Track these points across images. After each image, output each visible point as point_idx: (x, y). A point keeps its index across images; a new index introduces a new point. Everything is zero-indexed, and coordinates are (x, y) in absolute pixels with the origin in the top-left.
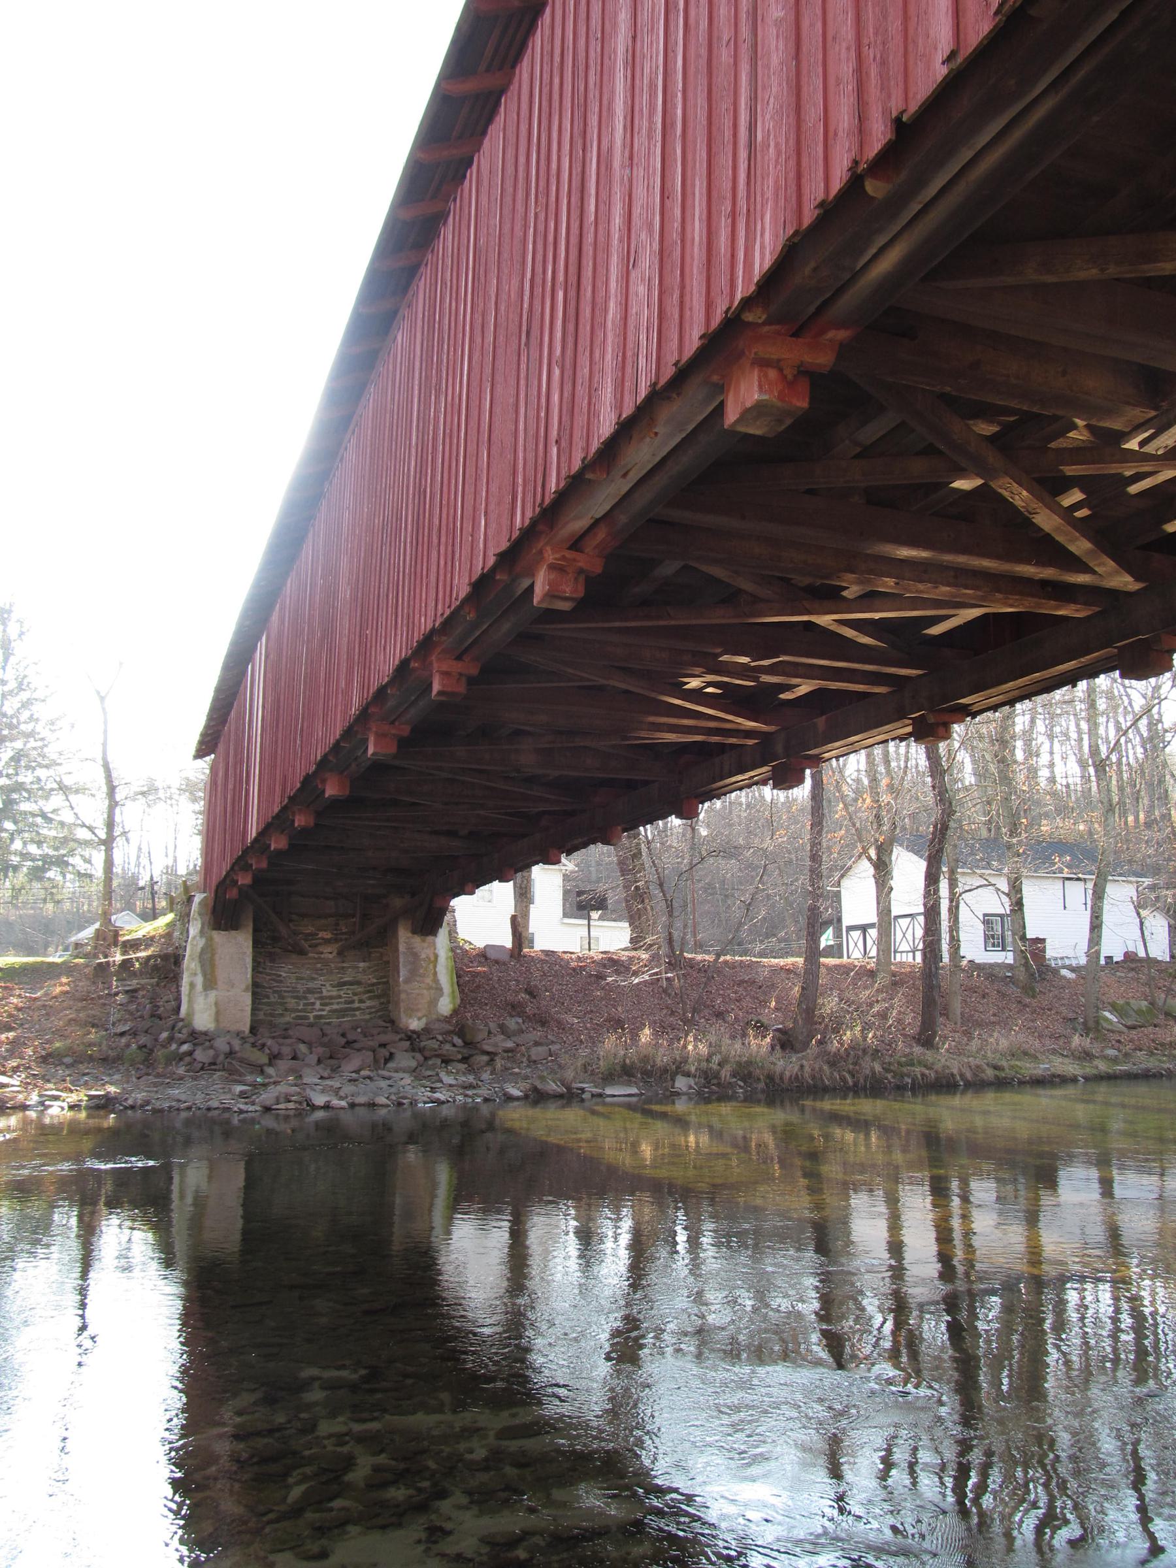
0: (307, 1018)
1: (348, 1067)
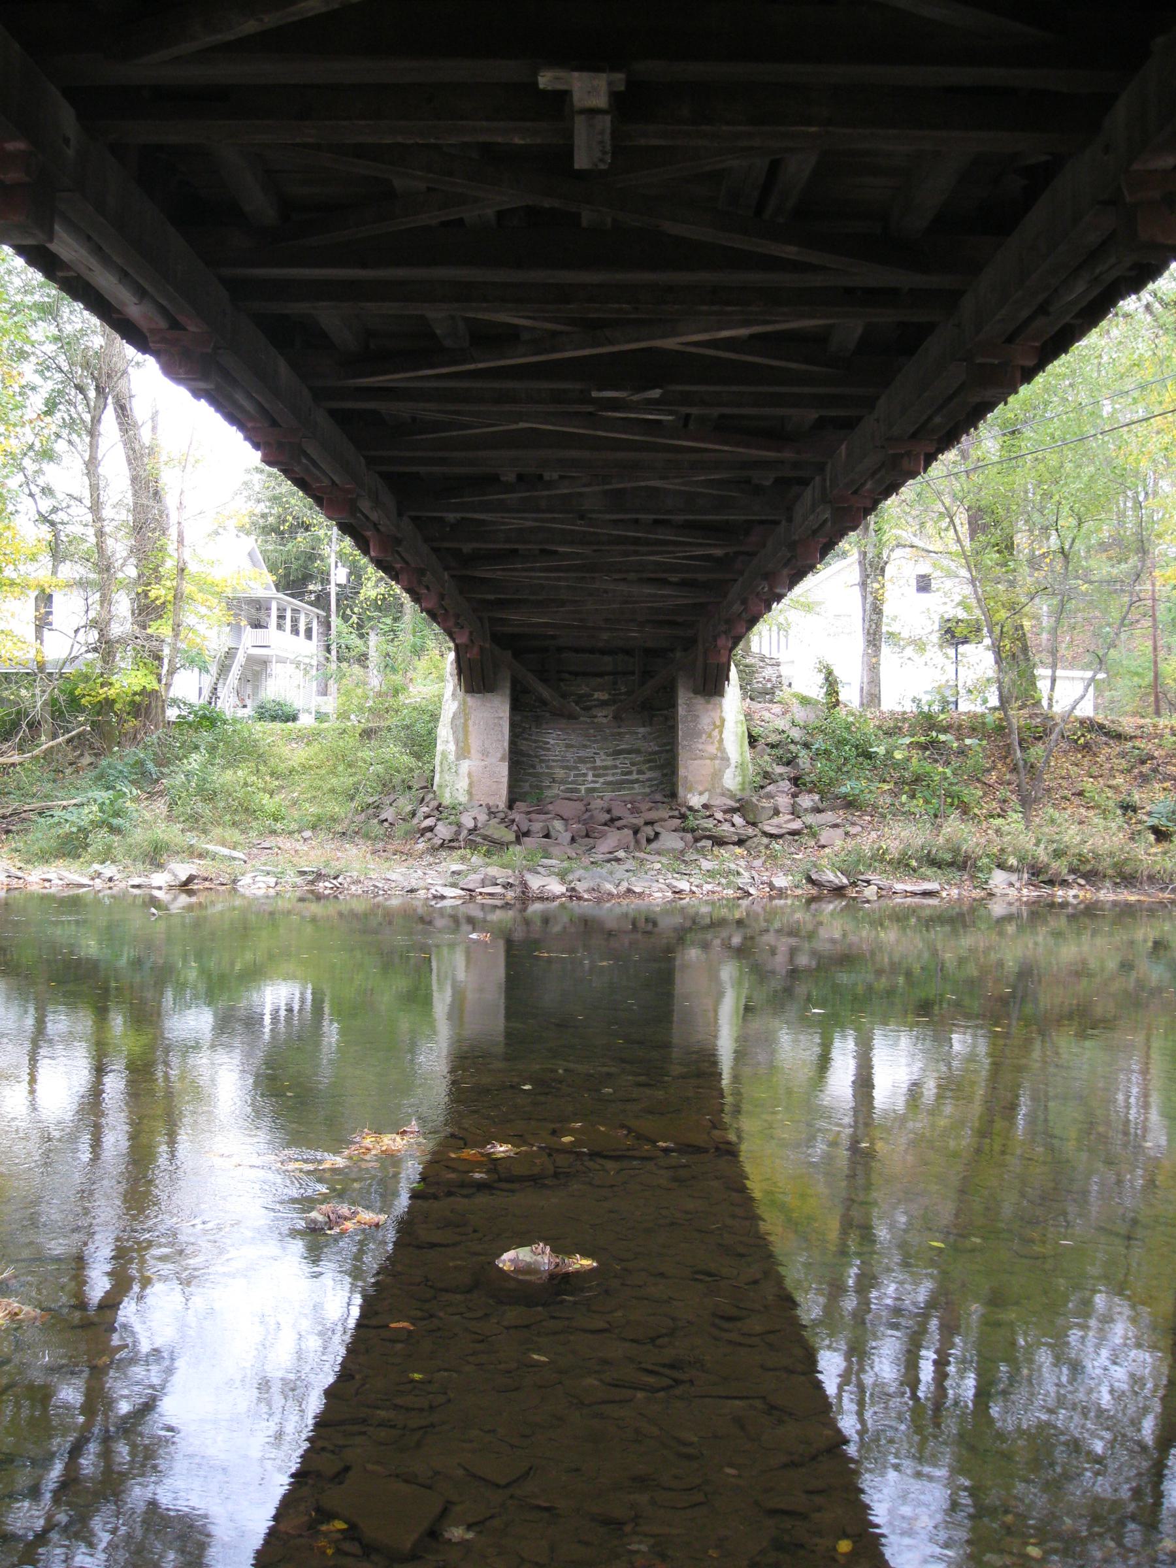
0: (577, 791)
1: (604, 846)
